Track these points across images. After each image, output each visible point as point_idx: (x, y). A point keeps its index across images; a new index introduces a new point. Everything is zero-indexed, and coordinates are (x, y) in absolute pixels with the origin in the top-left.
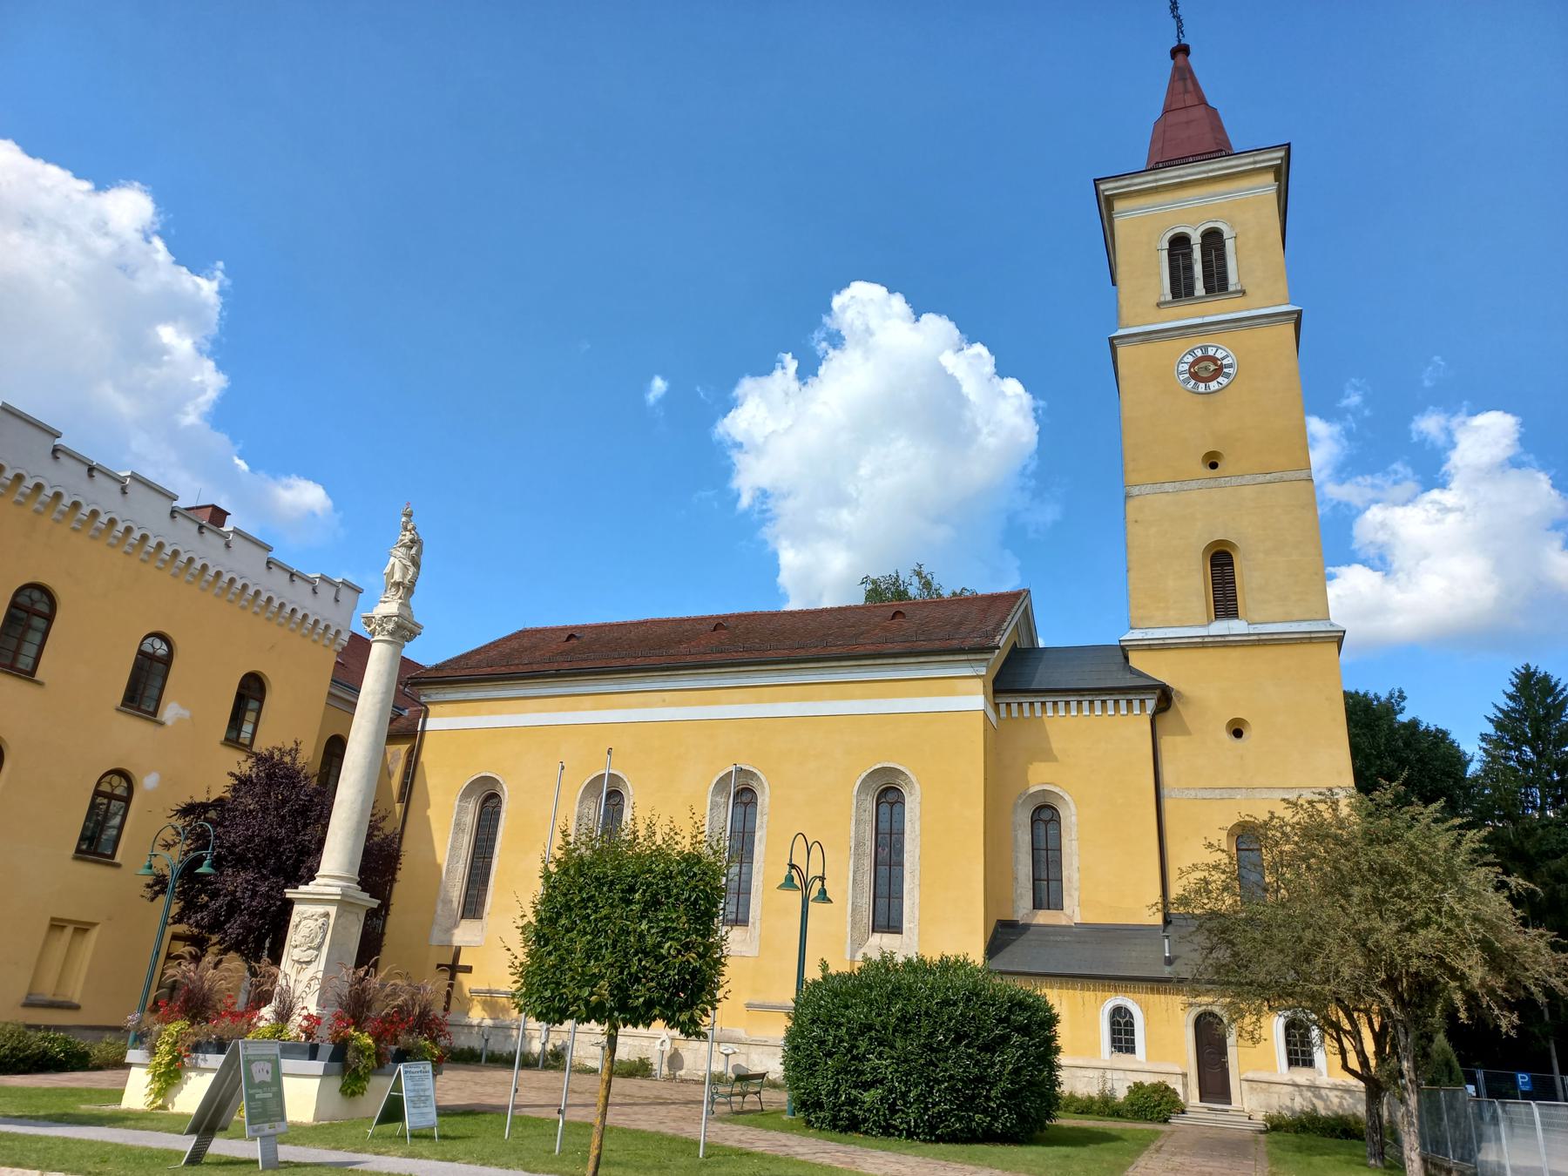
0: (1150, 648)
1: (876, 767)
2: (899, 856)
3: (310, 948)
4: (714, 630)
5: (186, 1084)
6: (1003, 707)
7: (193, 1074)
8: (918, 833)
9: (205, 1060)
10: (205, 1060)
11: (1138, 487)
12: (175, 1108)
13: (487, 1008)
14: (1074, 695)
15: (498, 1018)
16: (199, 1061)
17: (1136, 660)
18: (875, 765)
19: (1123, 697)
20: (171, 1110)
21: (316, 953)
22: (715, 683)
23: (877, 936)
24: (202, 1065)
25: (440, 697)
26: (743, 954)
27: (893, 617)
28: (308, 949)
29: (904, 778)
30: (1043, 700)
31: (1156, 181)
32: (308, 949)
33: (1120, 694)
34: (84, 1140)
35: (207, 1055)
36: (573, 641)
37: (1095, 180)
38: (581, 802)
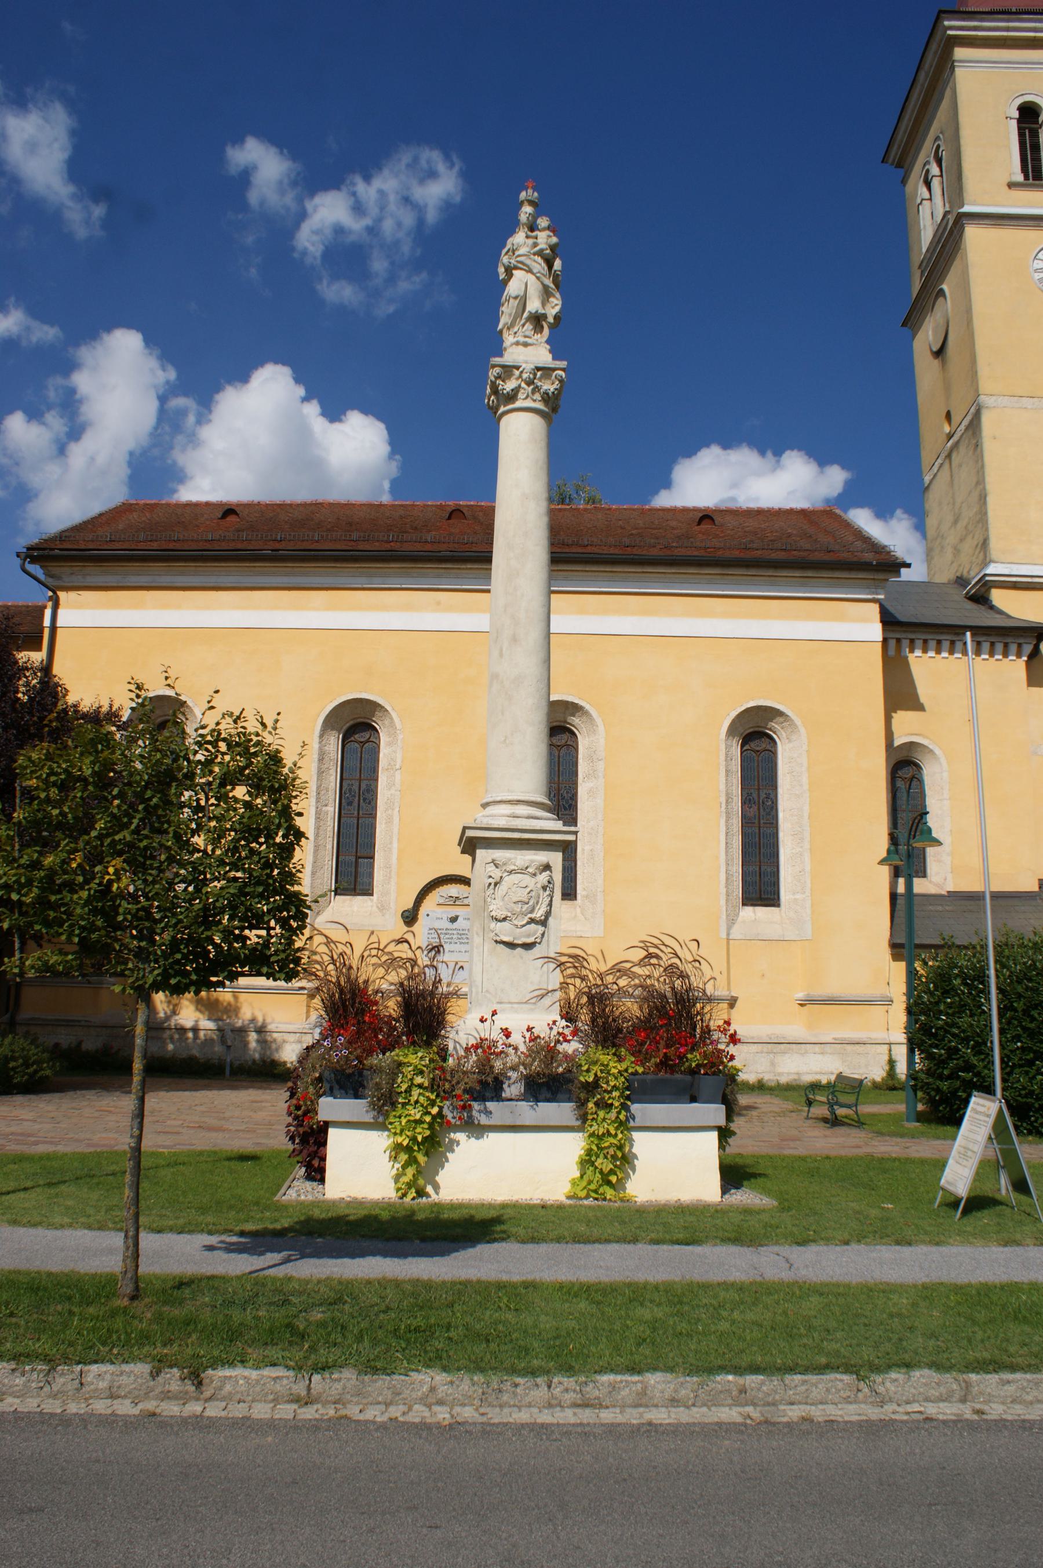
0: (1015, 586)
1: (749, 706)
2: (768, 814)
3: (532, 921)
4: (449, 518)
5: (453, 1151)
6: (892, 643)
7: (460, 1136)
8: (806, 787)
9: (488, 1113)
10: (488, 1113)
11: (994, 398)
12: (442, 1192)
13: (203, 1009)
14: (948, 633)
15: (221, 1020)
16: (475, 1113)
17: (998, 597)
18: (748, 702)
19: (1000, 639)
20: (434, 1197)
21: (540, 929)
22: (810, 575)
23: (749, 910)
24: (484, 1120)
25: (77, 580)
26: (579, 934)
27: (699, 523)
28: (528, 923)
29: (781, 719)
30: (898, 636)
31: (1008, 29)
32: (528, 923)
33: (997, 635)
34: (848, 1286)
35: (488, 1104)
36: (231, 518)
37: (941, 12)
38: (321, 736)
